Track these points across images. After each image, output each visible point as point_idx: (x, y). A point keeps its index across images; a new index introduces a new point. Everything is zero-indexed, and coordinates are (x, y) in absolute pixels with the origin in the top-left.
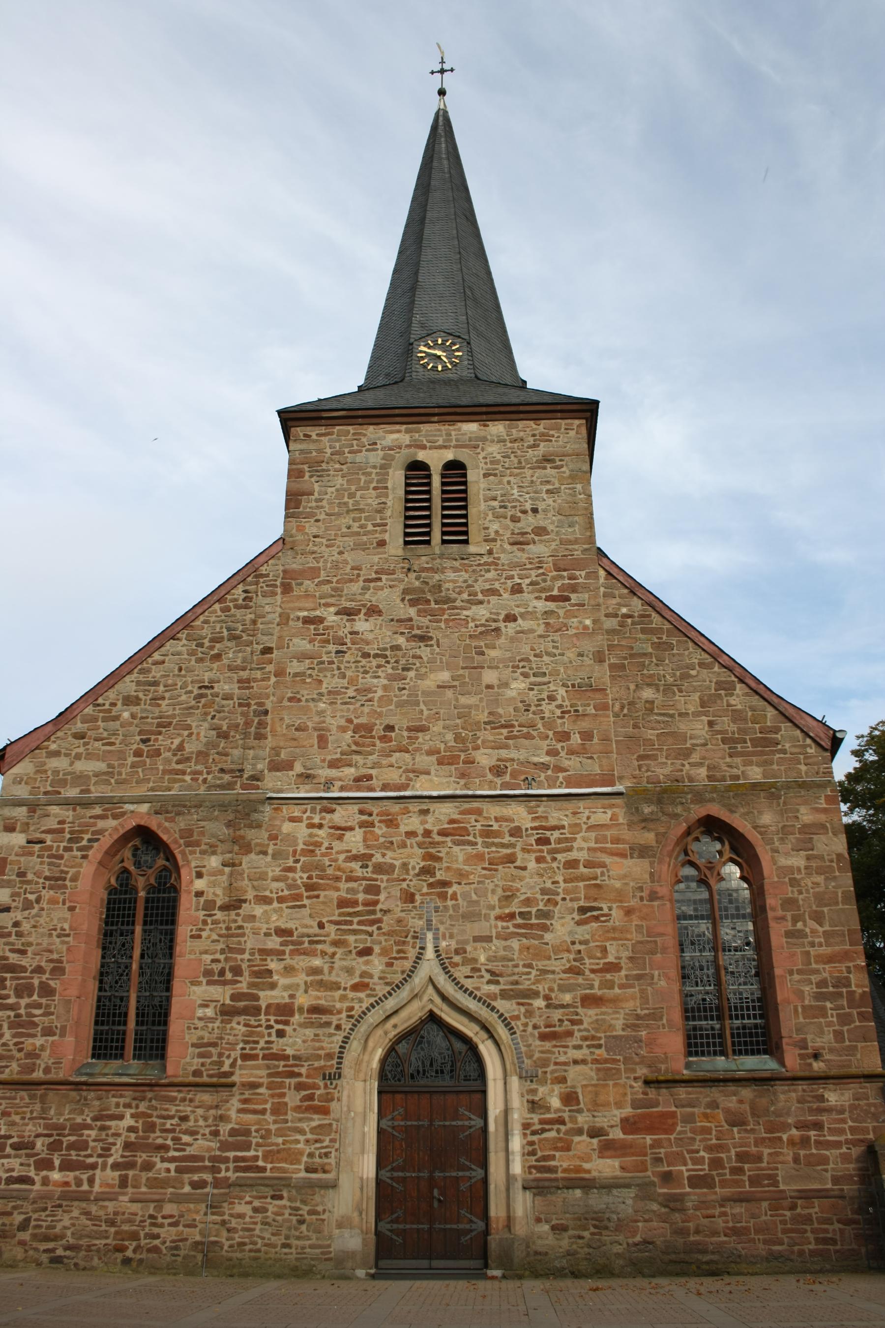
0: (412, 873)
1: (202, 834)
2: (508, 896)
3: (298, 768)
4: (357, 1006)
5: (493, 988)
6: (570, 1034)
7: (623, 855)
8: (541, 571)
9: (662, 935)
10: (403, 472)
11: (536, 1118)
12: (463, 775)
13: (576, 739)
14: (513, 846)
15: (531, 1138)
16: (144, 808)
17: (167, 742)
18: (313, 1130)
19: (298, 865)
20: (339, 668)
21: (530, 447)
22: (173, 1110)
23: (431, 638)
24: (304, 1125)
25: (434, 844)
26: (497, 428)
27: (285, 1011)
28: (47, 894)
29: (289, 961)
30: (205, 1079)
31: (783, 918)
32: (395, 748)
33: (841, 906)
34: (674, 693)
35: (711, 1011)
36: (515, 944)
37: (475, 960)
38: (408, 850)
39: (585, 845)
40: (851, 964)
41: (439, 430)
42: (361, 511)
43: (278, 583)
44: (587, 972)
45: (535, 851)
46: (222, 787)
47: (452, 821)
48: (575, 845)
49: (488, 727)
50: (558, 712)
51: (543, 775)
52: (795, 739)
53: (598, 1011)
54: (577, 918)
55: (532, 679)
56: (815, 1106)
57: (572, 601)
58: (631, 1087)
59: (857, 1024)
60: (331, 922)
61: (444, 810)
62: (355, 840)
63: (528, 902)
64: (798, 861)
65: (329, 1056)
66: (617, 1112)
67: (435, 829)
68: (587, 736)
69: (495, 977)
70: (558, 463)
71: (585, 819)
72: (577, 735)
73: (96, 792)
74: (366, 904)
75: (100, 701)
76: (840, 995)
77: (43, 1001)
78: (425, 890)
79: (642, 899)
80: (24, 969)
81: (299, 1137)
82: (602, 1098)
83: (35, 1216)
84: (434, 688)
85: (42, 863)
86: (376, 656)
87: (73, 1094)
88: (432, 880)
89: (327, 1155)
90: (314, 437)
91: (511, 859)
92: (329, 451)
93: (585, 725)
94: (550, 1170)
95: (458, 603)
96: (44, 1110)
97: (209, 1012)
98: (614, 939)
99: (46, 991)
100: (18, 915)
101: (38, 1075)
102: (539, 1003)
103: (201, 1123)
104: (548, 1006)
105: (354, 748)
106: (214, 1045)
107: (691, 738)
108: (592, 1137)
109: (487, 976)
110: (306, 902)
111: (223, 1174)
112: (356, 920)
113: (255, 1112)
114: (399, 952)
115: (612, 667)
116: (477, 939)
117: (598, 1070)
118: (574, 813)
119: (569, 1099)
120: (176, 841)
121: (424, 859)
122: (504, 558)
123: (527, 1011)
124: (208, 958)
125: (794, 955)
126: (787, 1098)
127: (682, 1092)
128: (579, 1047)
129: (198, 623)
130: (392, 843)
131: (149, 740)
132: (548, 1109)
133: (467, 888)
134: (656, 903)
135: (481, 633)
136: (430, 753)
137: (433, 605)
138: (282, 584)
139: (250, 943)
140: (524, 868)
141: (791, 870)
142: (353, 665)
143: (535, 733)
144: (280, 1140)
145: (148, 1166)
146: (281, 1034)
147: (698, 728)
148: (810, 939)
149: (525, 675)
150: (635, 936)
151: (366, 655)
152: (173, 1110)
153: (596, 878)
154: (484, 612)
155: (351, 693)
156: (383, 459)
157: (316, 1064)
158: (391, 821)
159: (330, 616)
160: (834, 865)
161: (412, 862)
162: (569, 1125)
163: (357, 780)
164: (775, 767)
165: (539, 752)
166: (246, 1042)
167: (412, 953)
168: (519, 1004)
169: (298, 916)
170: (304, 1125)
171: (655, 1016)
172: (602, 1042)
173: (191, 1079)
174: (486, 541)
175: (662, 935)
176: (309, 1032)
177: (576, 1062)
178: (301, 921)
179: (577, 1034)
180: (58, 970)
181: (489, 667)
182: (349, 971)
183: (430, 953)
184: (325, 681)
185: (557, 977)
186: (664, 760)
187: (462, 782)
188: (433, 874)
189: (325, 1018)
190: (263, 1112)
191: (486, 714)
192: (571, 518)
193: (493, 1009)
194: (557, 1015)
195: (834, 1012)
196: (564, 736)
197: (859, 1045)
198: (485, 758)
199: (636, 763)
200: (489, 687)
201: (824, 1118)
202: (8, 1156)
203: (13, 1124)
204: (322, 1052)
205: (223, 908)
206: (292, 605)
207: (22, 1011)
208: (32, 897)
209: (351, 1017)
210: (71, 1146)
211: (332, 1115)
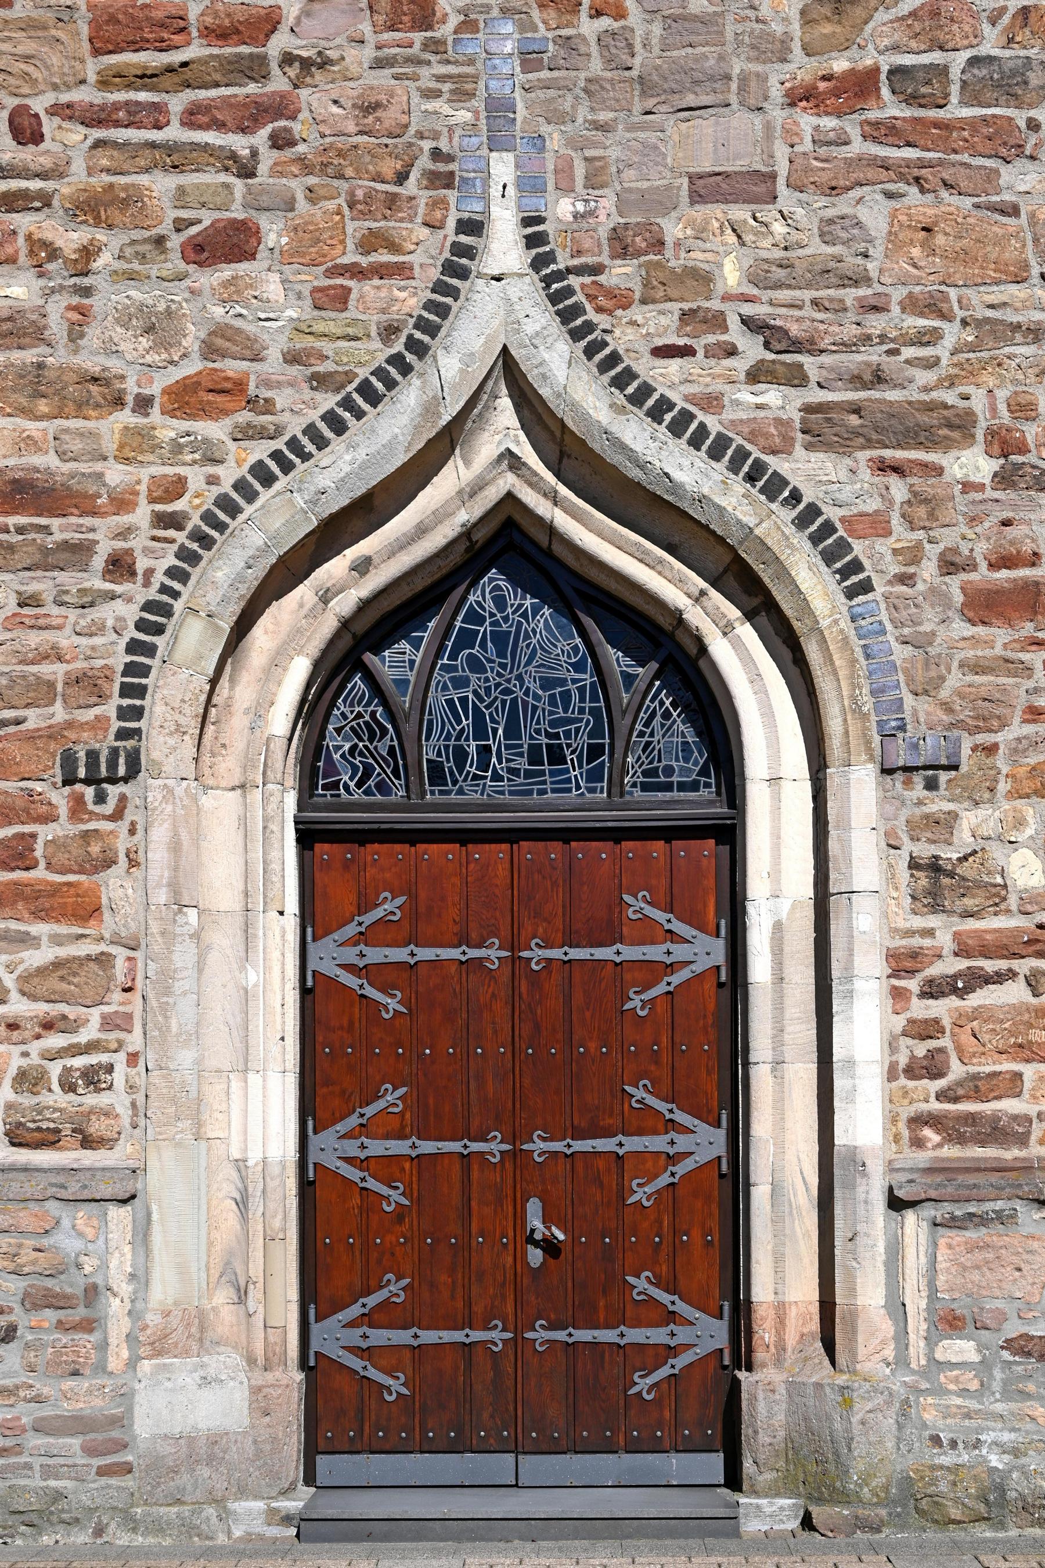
4: (195, 477)
11: (944, 931)
15: (922, 1009)
36: (874, 213)
37: (702, 279)
60: (64, 111)
65: (87, 685)
69: (783, 352)
94: (997, 1131)
102: (972, 463)
104: (1004, 479)
109: (752, 350)
112: (177, 103)
116: (708, 188)
123: (917, 498)
132: (997, 896)
167: (426, 250)
168: (883, 467)
182: (157, 327)
183: (504, 248)
189: (61, 529)
193: (774, 486)
204: (55, 671)
209: (174, 521)
211: (109, 924)
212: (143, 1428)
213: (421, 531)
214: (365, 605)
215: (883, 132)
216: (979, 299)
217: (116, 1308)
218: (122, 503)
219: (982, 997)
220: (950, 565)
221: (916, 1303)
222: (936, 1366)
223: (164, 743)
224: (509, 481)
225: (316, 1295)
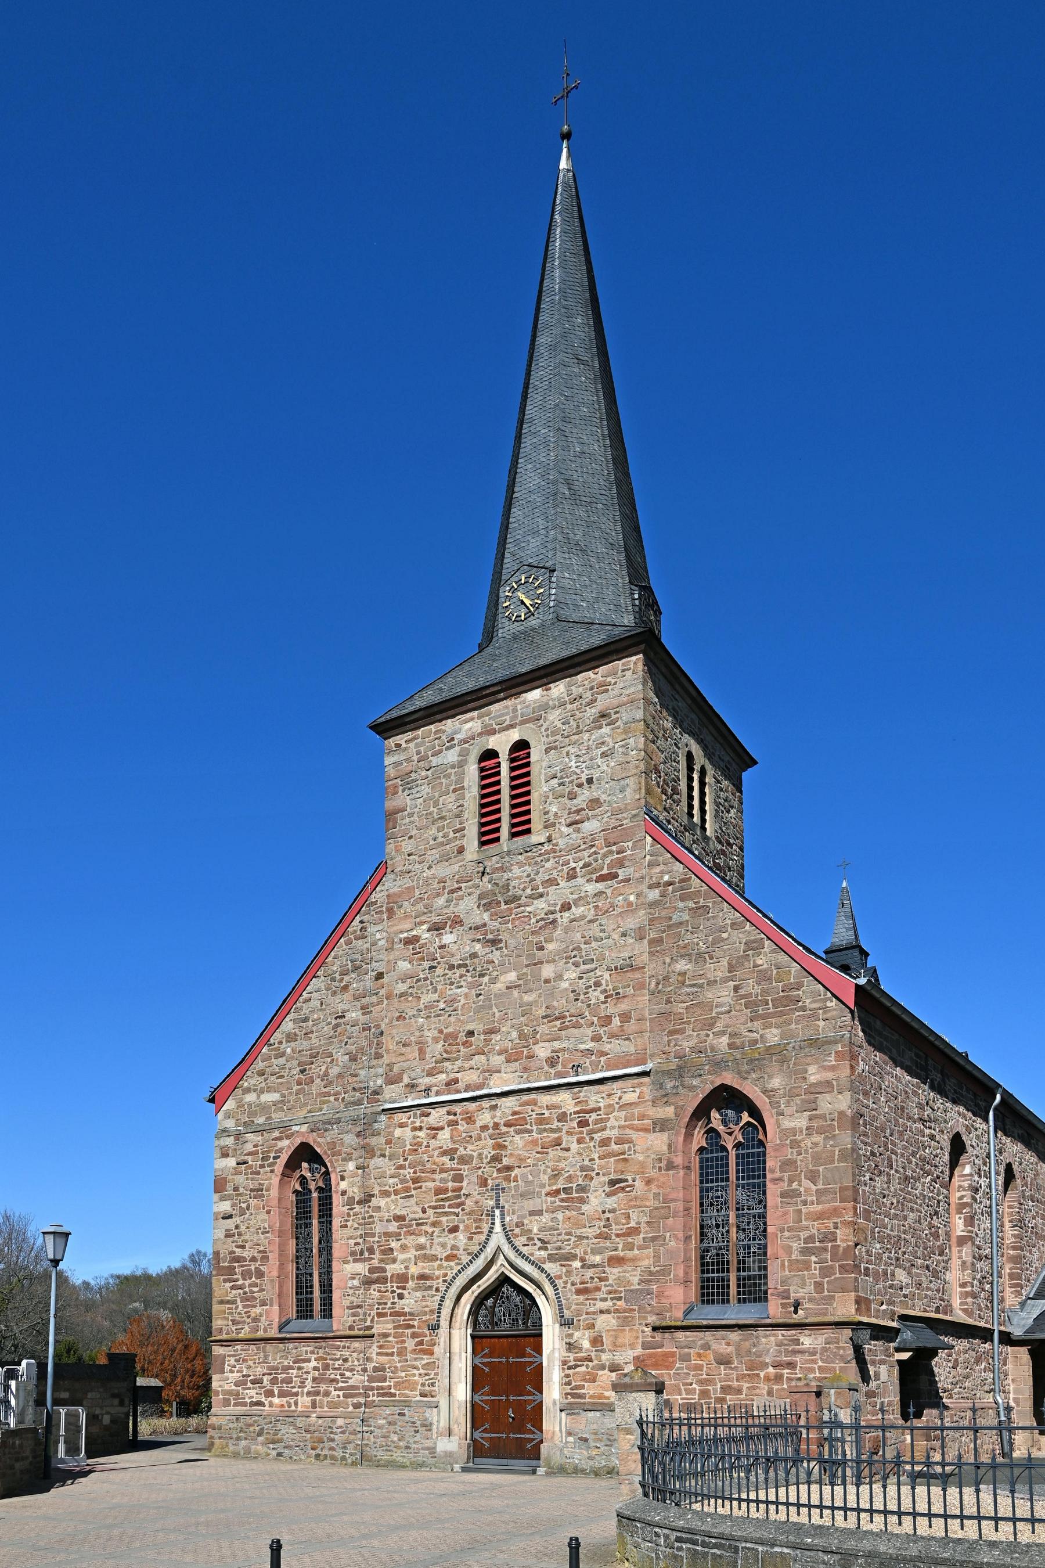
0: (485, 1161)
1: (342, 1144)
2: (556, 1175)
3: (406, 1080)
4: (449, 1272)
5: (543, 1254)
6: (598, 1289)
7: (646, 1130)
8: (593, 850)
9: (675, 1200)
10: (476, 766)
11: (572, 1356)
12: (525, 1070)
13: (616, 1021)
14: (559, 1130)
15: (568, 1372)
16: (304, 1128)
17: (317, 1069)
18: (424, 1366)
19: (407, 1163)
20: (432, 984)
21: (588, 704)
22: (338, 1354)
23: (501, 941)
24: (417, 1363)
25: (501, 1135)
26: (559, 689)
27: (402, 1279)
28: (253, 1202)
29: (403, 1241)
30: (356, 1332)
31: (781, 1179)
32: (473, 1052)
33: (836, 1164)
34: (705, 961)
35: (713, 1265)
36: (560, 1216)
37: (530, 1231)
38: (483, 1142)
39: (616, 1124)
40: (838, 1220)
41: (507, 707)
42: (443, 818)
43: (384, 909)
44: (613, 1237)
45: (576, 1134)
46: (354, 1104)
47: (514, 1113)
48: (609, 1124)
49: (545, 1021)
50: (602, 998)
51: (588, 1061)
52: (815, 994)
53: (620, 1269)
54: (607, 1190)
55: (583, 967)
56: (790, 1348)
57: (620, 878)
58: (643, 1331)
59: (838, 1275)
60: (430, 1207)
61: (509, 1104)
62: (445, 1135)
63: (570, 1179)
64: (801, 1122)
65: (432, 1312)
66: (630, 1352)
67: (502, 1122)
68: (625, 1017)
69: (544, 1244)
70: (614, 717)
71: (617, 1100)
72: (617, 1018)
73: (276, 1116)
74: (453, 1191)
75: (272, 1041)
76: (825, 1249)
77: (258, 1281)
78: (495, 1175)
79: (660, 1168)
80: (244, 1259)
81: (415, 1372)
82: (620, 1341)
83: (266, 1427)
84: (504, 990)
85: (247, 1179)
86: (460, 966)
87: (281, 1345)
88: (499, 1166)
89: (433, 1385)
90: (404, 745)
91: (558, 1143)
92: (416, 758)
93: (624, 1006)
94: (580, 1396)
95: (523, 900)
96: (266, 1357)
97: (356, 1283)
98: (636, 1206)
99: (260, 1274)
100: (237, 1220)
101: (260, 1334)
102: (577, 1264)
103: (356, 1363)
104: (583, 1267)
105: (445, 1055)
106: (360, 1307)
107: (717, 1007)
108: (612, 1371)
109: (539, 1244)
110: (413, 1192)
111: (371, 1398)
112: (447, 1204)
113: (387, 1354)
114: (477, 1228)
115: (652, 942)
116: (532, 1213)
117: (618, 1318)
118: (609, 1095)
119: (597, 1341)
120: (325, 1153)
121: (494, 1149)
122: (562, 842)
123: (567, 1271)
124: (352, 1242)
125: (785, 1214)
126: (769, 1342)
127: (681, 1335)
128: (605, 1300)
129: (330, 959)
130: (471, 1137)
131: (305, 1070)
132: (581, 1349)
133: (525, 1170)
134: (671, 1172)
135: (540, 928)
136: (500, 1053)
137: (503, 907)
138: (388, 910)
139: (378, 1228)
140: (568, 1150)
141: (793, 1131)
142: (442, 979)
143: (582, 1021)
144: (403, 1374)
145: (327, 1394)
146: (401, 1297)
147: (724, 995)
148: (803, 1198)
149: (576, 965)
150: (651, 1203)
151: (452, 967)
152: (338, 1354)
153: (623, 1153)
154: (543, 906)
155: (442, 1005)
156: (460, 755)
157: (424, 1318)
158: (470, 1118)
159: (422, 932)
160: (836, 1123)
161: (485, 1152)
162: (596, 1362)
163: (448, 1084)
164: (793, 1026)
165: (585, 1039)
166: (379, 1304)
167: (486, 1228)
168: (562, 1265)
169: (408, 1204)
170: (417, 1363)
171: (665, 1271)
172: (622, 1295)
173: (348, 1333)
174: (545, 827)
175: (675, 1200)
176: (419, 1294)
177: (602, 1312)
178: (410, 1209)
179: (604, 1289)
180: (265, 1259)
181: (547, 962)
182: (443, 1245)
183: (498, 1227)
184: (423, 997)
185: (591, 1241)
186: (691, 1033)
187: (525, 1076)
188: (500, 1161)
189: (428, 1283)
190: (392, 1354)
191: (544, 1009)
192: (622, 782)
193: (542, 1270)
194: (589, 1273)
195: (818, 1266)
196: (607, 1020)
197: (837, 1295)
198: (543, 1051)
199: (666, 1039)
200: (547, 981)
201: (798, 1359)
202: (249, 1388)
203: (249, 1367)
204: (427, 1309)
205: (360, 1203)
206: (395, 928)
207: (247, 1290)
208: (244, 1206)
209: (445, 1281)
210: (283, 1381)
211: (435, 1356)
212: (438, 1450)
213: (489, 1279)
214: (479, 1294)
215: (562, 1200)
216: (579, 1232)
217: (434, 1427)
218: (438, 1278)
219: (578, 1370)
220: (573, 1284)
221: (564, 1430)
222: (567, 1442)
223: (444, 1323)
224: (503, 1269)
225: (474, 1427)
